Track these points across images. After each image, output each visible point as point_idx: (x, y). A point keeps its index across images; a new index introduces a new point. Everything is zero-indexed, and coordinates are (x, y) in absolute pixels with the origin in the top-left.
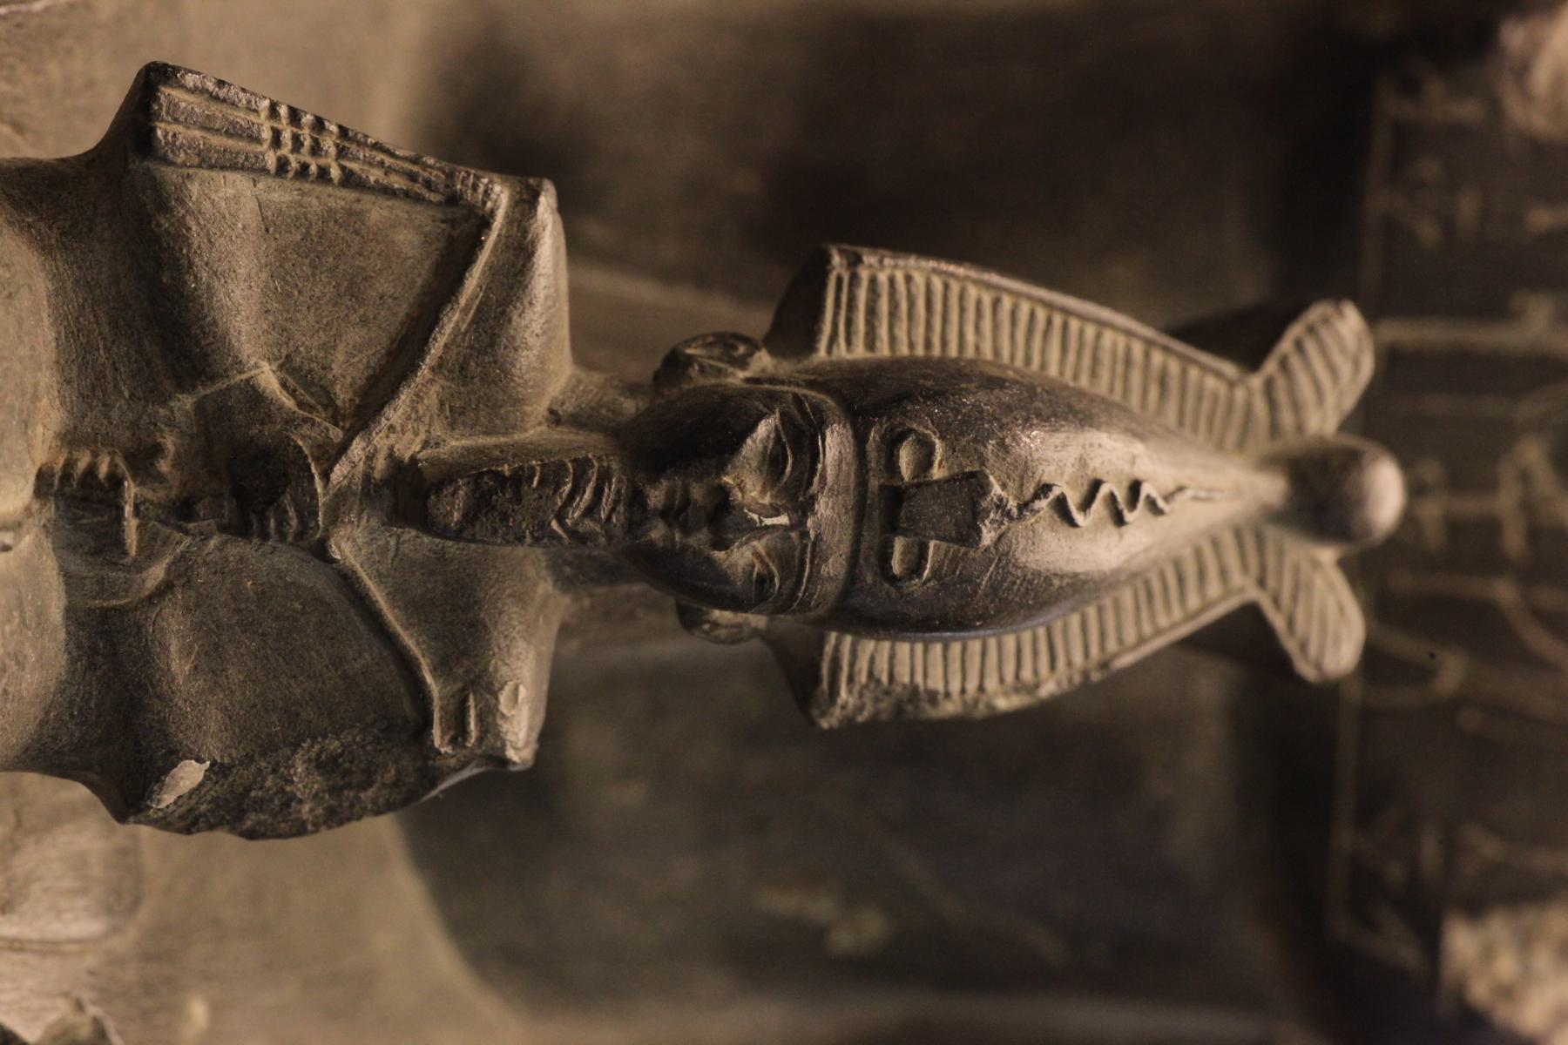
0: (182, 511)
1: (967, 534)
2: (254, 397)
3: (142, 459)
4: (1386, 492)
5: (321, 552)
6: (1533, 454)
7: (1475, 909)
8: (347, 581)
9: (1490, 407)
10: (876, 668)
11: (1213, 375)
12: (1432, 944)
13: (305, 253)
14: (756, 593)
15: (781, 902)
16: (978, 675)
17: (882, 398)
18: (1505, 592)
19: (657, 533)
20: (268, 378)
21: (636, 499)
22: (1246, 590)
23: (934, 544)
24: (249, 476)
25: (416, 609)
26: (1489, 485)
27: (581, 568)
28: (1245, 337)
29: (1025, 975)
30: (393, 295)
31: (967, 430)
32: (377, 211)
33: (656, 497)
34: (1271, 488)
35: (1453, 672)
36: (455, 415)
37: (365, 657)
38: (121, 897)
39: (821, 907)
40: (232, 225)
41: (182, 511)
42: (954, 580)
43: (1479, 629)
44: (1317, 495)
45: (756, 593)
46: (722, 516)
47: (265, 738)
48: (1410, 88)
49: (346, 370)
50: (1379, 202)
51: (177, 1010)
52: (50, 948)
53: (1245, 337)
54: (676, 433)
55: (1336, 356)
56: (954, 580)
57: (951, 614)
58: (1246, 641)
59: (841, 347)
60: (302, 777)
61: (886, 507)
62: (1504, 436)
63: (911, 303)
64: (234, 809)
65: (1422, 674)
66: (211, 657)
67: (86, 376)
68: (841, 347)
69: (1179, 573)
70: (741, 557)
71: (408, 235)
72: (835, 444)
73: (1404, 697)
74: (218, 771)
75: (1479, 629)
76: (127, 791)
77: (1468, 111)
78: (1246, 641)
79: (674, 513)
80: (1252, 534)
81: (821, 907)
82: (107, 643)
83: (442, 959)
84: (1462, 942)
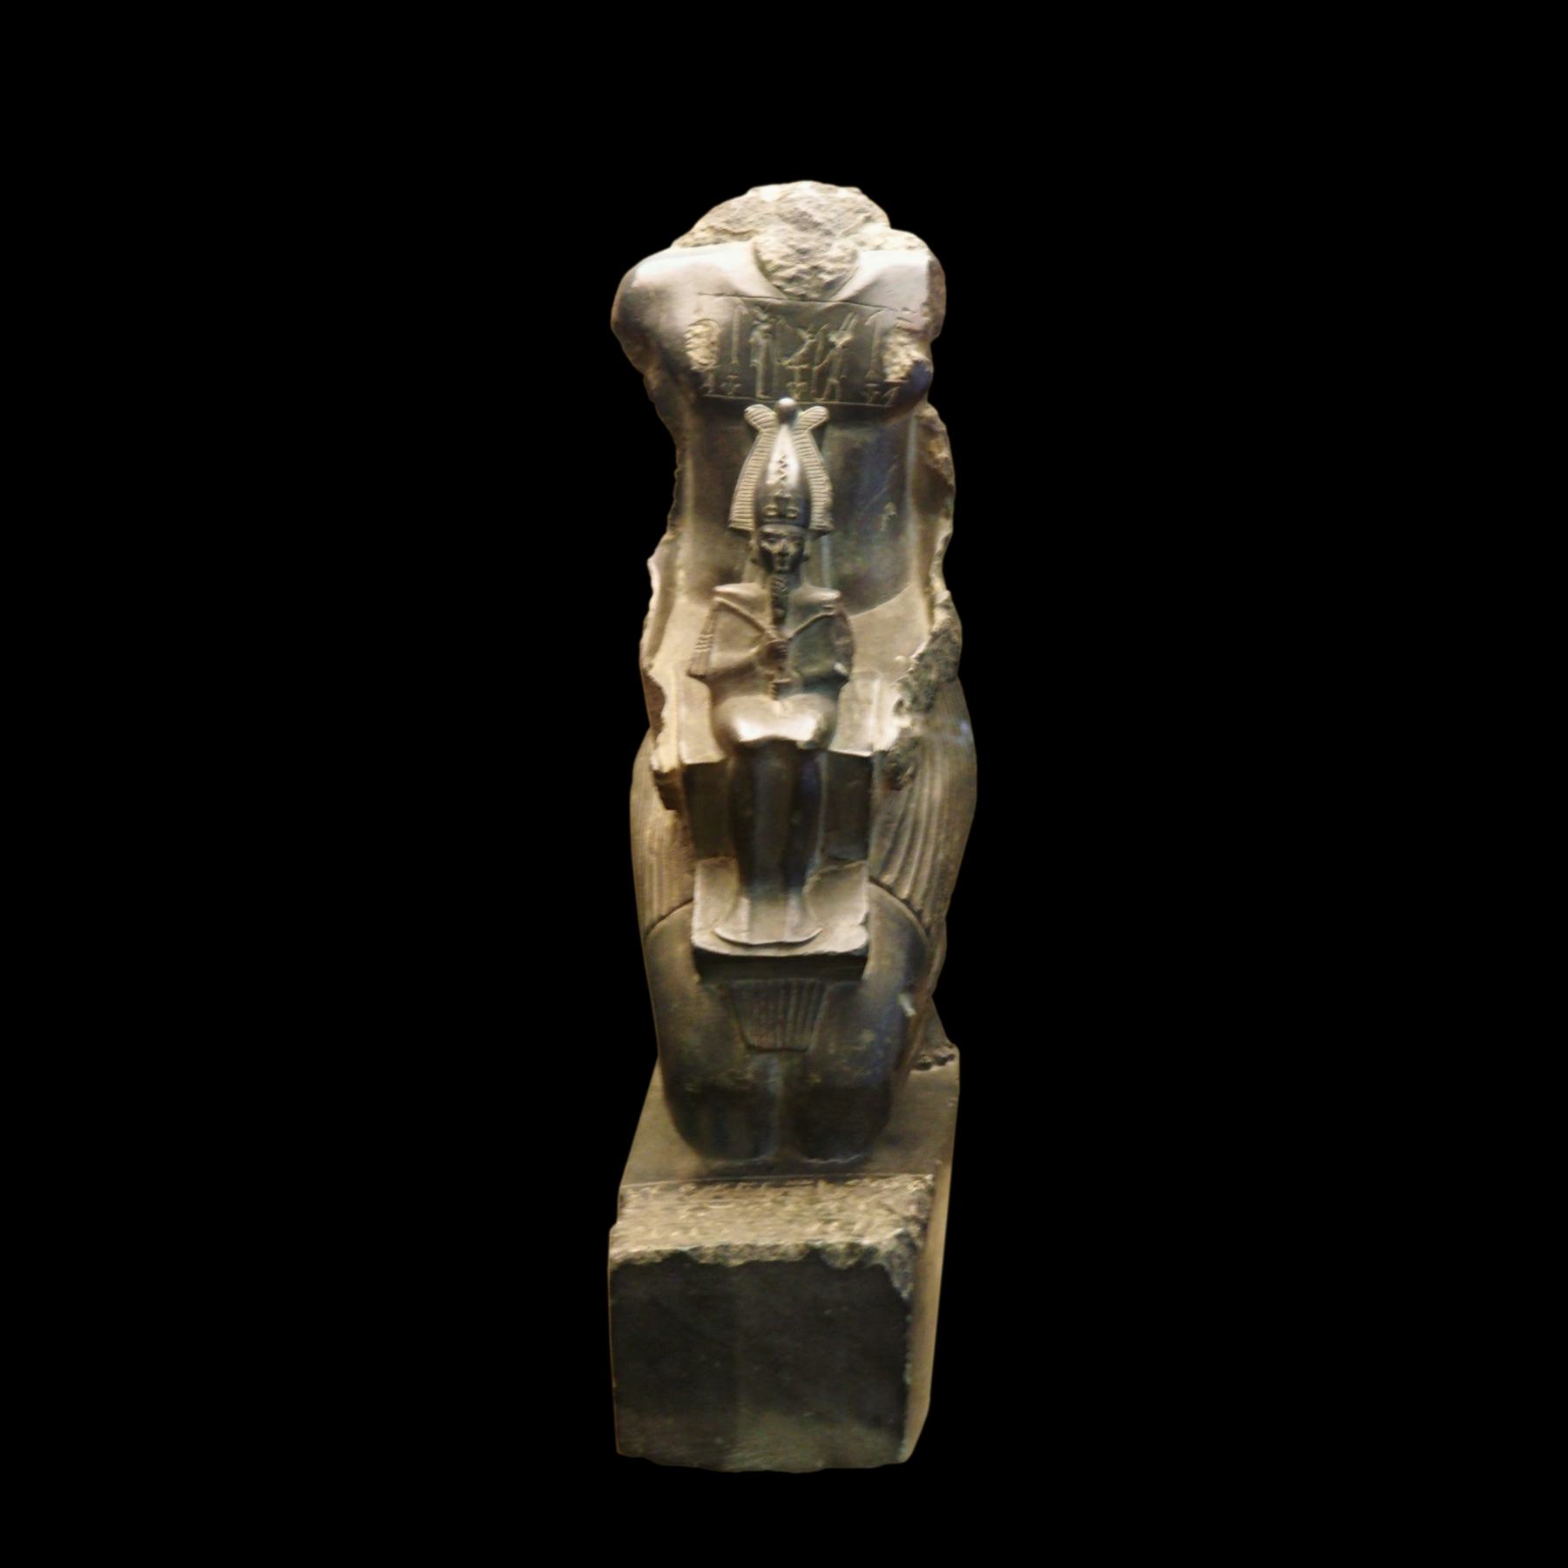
0: (781, 669)
1: (787, 500)
2: (758, 654)
3: (771, 678)
4: (786, 402)
5: (790, 639)
6: (786, 362)
7: (884, 376)
8: (799, 633)
9: (775, 372)
10: (819, 518)
11: (761, 440)
12: (892, 385)
13: (728, 640)
14: (801, 546)
15: (883, 526)
16: (822, 494)
17: (760, 519)
18: (816, 368)
19: (787, 567)
20: (754, 650)
21: (780, 572)
22: (806, 433)
23: (790, 508)
24: (774, 655)
25: (804, 617)
26: (792, 371)
27: (797, 582)
28: (753, 432)
29: (901, 473)
30: (737, 623)
31: (766, 500)
32: (720, 626)
33: (778, 568)
34: (784, 429)
35: (833, 380)
36: (762, 610)
37: (814, 629)
38: (870, 676)
39: (885, 518)
40: (720, 658)
41: (781, 669)
42: (797, 502)
43: (824, 374)
44: (787, 417)
45: (801, 546)
46: (783, 554)
47: (831, 651)
48: (707, 389)
49: (752, 633)
50: (730, 397)
51: (898, 663)
52: (881, 693)
53: (753, 432)
54: (766, 561)
55: (758, 413)
56: (797, 502)
57: (807, 503)
58: (819, 432)
59: (749, 525)
60: (840, 642)
61: (781, 517)
62: (782, 368)
63: (741, 511)
64: (848, 657)
65: (833, 387)
66: (812, 662)
67: (753, 689)
68: (749, 525)
69: (801, 450)
70: (792, 549)
71: (725, 619)
72: (768, 529)
73: (838, 390)
74: (839, 660)
75: (824, 374)
76: (841, 680)
77: (711, 376)
78: (819, 432)
79: (782, 564)
80: (794, 431)
81: (885, 518)
82: (809, 685)
83: (894, 601)
84: (892, 378)
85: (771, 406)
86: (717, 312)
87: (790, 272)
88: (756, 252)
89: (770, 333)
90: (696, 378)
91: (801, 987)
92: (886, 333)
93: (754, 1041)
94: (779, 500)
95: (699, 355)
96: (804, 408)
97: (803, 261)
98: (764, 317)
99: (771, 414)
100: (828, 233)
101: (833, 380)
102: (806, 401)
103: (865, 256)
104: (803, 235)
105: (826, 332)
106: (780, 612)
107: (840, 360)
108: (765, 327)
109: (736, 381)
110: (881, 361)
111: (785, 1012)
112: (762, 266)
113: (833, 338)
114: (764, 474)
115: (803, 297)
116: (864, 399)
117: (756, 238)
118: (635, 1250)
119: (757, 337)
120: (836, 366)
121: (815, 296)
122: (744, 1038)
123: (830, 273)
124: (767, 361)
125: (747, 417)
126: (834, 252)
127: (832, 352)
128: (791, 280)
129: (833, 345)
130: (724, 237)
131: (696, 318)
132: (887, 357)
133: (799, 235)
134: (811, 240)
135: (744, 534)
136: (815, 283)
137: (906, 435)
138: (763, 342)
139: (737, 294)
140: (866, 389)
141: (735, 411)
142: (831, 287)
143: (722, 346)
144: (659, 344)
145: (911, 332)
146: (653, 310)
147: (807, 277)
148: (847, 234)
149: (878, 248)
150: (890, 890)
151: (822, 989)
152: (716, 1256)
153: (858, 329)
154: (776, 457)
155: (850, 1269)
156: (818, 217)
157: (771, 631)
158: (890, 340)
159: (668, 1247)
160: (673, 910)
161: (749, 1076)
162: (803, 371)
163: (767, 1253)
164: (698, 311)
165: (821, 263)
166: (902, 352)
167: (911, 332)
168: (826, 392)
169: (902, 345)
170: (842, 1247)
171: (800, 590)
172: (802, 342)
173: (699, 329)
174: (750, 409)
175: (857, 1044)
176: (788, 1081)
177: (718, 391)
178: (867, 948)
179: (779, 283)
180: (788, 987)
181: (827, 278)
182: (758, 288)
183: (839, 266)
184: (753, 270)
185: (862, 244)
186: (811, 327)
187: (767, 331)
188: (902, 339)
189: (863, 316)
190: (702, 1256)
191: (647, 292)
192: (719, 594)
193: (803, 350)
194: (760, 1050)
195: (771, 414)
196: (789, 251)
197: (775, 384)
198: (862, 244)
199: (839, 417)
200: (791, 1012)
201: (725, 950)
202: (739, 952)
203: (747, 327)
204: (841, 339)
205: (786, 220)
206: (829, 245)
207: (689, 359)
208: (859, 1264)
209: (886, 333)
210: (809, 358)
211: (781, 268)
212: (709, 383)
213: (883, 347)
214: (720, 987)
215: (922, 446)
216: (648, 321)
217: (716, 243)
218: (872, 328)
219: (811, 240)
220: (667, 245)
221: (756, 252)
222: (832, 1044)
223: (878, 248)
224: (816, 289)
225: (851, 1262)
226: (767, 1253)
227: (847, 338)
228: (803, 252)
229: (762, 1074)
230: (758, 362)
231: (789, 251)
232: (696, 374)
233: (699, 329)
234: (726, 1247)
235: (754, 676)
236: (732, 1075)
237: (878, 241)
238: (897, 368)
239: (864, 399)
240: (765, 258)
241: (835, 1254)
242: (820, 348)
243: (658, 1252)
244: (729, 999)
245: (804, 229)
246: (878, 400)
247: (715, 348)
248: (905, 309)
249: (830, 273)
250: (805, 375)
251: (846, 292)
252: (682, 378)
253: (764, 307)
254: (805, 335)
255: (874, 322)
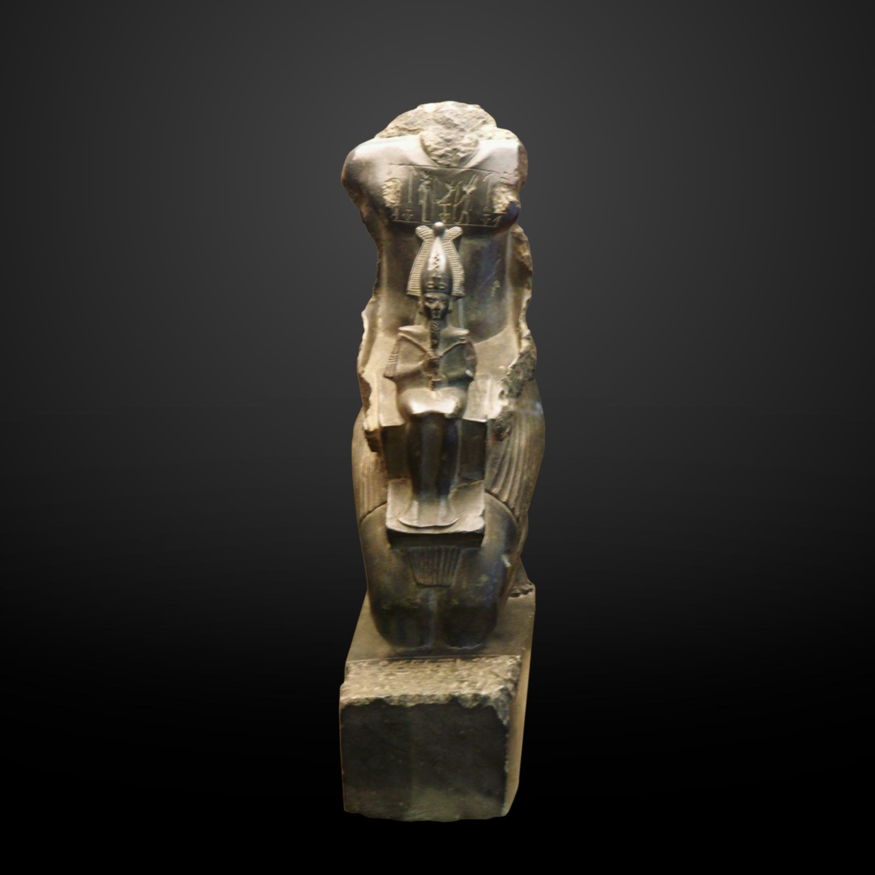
0: (436, 373)
1: (439, 279)
2: (423, 365)
3: (430, 378)
4: (439, 224)
5: (441, 357)
6: (439, 202)
7: (494, 210)
8: (446, 353)
9: (433, 208)
10: (457, 289)
11: (425, 246)
12: (498, 215)
13: (407, 357)
14: (447, 305)
15: (493, 294)
16: (458, 276)
17: (424, 289)
18: (455, 205)
19: (439, 317)
20: (421, 363)
21: (435, 319)
22: (450, 242)
23: (441, 284)
24: (432, 365)
25: (449, 344)
26: (442, 207)
27: (445, 325)
28: (420, 241)
29: (503, 264)
30: (412, 347)
31: (427, 279)
32: (402, 349)
33: (434, 317)
34: (438, 239)
35: (465, 212)
36: (425, 340)
37: (454, 351)
38: (486, 377)
39: (494, 289)
40: (402, 367)
41: (436, 373)
42: (445, 280)
43: (460, 209)
44: (439, 233)
45: (447, 305)
46: (437, 309)
47: (464, 363)
48: (394, 217)
49: (420, 353)
50: (408, 221)
51: (501, 370)
52: (492, 387)
53: (420, 241)
54: (428, 313)
55: (423, 230)
56: (445, 280)
57: (450, 281)
58: (457, 241)
59: (418, 293)
60: (469, 358)
61: (436, 289)
62: (436, 205)
63: (414, 285)
64: (473, 366)
65: (465, 216)
66: (453, 370)
67: (420, 385)
68: (418, 293)
69: (447, 251)
70: (442, 306)
71: (405, 346)
72: (429, 295)
73: (468, 218)
74: (468, 369)
75: (460, 209)
76: (469, 379)
77: (397, 210)
78: (457, 241)
79: (437, 315)
80: (443, 240)
81: (494, 289)
82: (452, 382)
83: (499, 335)
84: (498, 211)
89: (430, 186)
90: (389, 211)
91: (447, 551)
93: (421, 581)
94: (434, 279)
95: (390, 198)
96: (449, 228)
97: (448, 146)
98: (426, 177)
101: (465, 212)
102: (450, 224)
105: (461, 185)
106: (435, 341)
107: (469, 201)
108: (427, 182)
110: (491, 202)
111: (438, 565)
113: (465, 189)
114: (426, 264)
115: (448, 166)
116: (482, 223)
118: (354, 697)
119: (423, 188)
121: (455, 165)
122: (415, 579)
123: (463, 152)
124: (428, 201)
127: (464, 197)
128: (441, 156)
129: (465, 193)
130: (404, 132)
131: (389, 177)
132: (495, 199)
134: (452, 134)
135: (415, 298)
136: (455, 158)
138: (426, 191)
139: (411, 164)
142: (464, 160)
143: (403, 193)
150: (497, 497)
151: (459, 552)
152: (399, 701)
153: (479, 184)
154: (433, 255)
155: (475, 708)
156: (456, 121)
157: (430, 352)
159: (372, 696)
160: (376, 508)
161: (418, 601)
162: (448, 207)
163: (428, 699)
165: (458, 147)
168: (461, 219)
170: (470, 696)
171: (446, 329)
172: (448, 191)
173: (390, 184)
175: (478, 583)
176: (439, 604)
177: (401, 218)
179: (435, 158)
180: (439, 551)
186: (453, 182)
190: (392, 701)
192: (401, 331)
193: (448, 196)
194: (424, 586)
197: (433, 214)
200: (442, 565)
201: (405, 530)
202: (412, 531)
204: (469, 189)
205: (439, 123)
206: (463, 137)
208: (480, 706)
209: (494, 186)
211: (436, 149)
212: (396, 214)
214: (402, 551)
217: (400, 135)
220: (372, 137)
222: (464, 583)
224: (455, 161)
225: (475, 704)
226: (428, 699)
227: (473, 188)
228: (448, 141)
229: (425, 599)
230: (423, 202)
231: (440, 140)
232: (388, 209)
233: (390, 184)
234: (405, 696)
235: (421, 377)
236: (408, 600)
241: (466, 700)
242: (458, 194)
243: (367, 699)
244: (407, 558)
245: (449, 128)
247: (399, 194)
249: (463, 152)
250: (449, 209)
251: (472, 163)
252: (381, 211)
253: (426, 171)
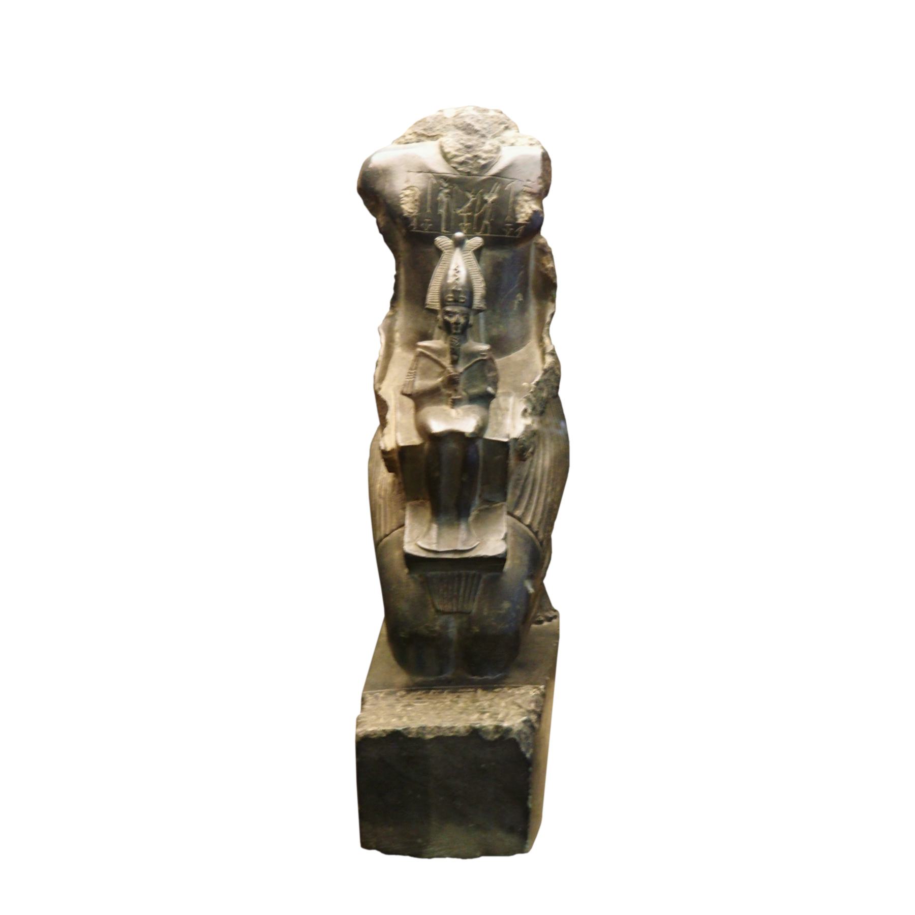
0: (456, 391)
1: (459, 292)
2: (442, 381)
3: (450, 395)
4: (459, 235)
5: (461, 373)
6: (459, 211)
7: (516, 219)
8: (466, 369)
9: (452, 217)
10: (478, 302)
11: (444, 257)
12: (521, 224)
13: (425, 374)
14: (467, 319)
15: (516, 307)
16: (479, 288)
17: (444, 303)
18: (476, 215)
19: (459, 331)
20: (440, 379)
21: (455, 334)
22: (470, 253)
23: (461, 297)
24: (452, 382)
25: (469, 360)
26: (462, 217)
27: (465, 339)
28: (439, 252)
29: (526, 276)
30: (430, 363)
31: (447, 292)
32: (420, 365)
33: (454, 331)
34: (458, 250)
35: (486, 222)
36: (444, 356)
37: (475, 367)
38: (508, 394)
39: (516, 302)
40: (420, 384)
41: (456, 391)
42: (465, 293)
43: (481, 218)
44: (459, 243)
45: (467, 319)
46: (457, 323)
47: (485, 380)
48: (412, 227)
49: (439, 370)
50: (426, 231)
51: (524, 387)
52: (514, 404)
53: (439, 252)
54: (447, 328)
55: (442, 241)
56: (465, 293)
57: (471, 294)
58: (478, 252)
59: (437, 306)
60: (490, 375)
61: (456, 302)
62: (456, 215)
63: (433, 298)
64: (495, 383)
65: (486, 226)
66: (474, 386)
67: (439, 402)
68: (437, 306)
69: (468, 262)
70: (462, 320)
71: (423, 361)
72: (448, 309)
73: (489, 228)
74: (489, 385)
75: (481, 218)
76: (491, 397)
77: (415, 220)
78: (478, 252)
79: (457, 329)
80: (464, 251)
81: (516, 302)
82: (472, 399)
83: (522, 350)
84: (520, 221)
85: (450, 237)
86: (418, 182)
87: (461, 159)
88: (441, 147)
89: (449, 194)
90: (406, 220)
91: (467, 576)
92: (517, 194)
93: (440, 607)
94: (454, 292)
96: (469, 238)
97: (468, 152)
98: (446, 185)
99: (450, 242)
100: (483, 136)
101: (486, 222)
102: (470, 234)
103: (505, 149)
104: (469, 137)
105: (482, 194)
106: (455, 357)
107: (490, 210)
108: (447, 191)
109: (429, 223)
110: (514, 211)
111: (458, 591)
112: (445, 155)
113: (486, 197)
114: (446, 277)
115: (469, 174)
116: (504, 233)
117: (441, 139)
118: (370, 729)
119: (442, 196)
120: (488, 214)
121: (475, 172)
122: (434, 606)
123: (484, 159)
124: (448, 211)
125: (436, 243)
126: (487, 147)
127: (485, 206)
128: (462, 163)
129: (486, 201)
130: (422, 138)
131: (406, 185)
132: (518, 208)
133: (466, 137)
134: (473, 140)
135: (434, 312)
136: (475, 165)
137: (529, 254)
138: (445, 200)
139: (430, 172)
140: (505, 227)
141: (429, 240)
142: (485, 167)
143: (422, 202)
144: (385, 201)
145: (532, 194)
146: (381, 181)
147: (471, 162)
148: (494, 136)
149: (512, 145)
150: (520, 519)
151: (480, 577)
152: (418, 733)
153: (500, 192)
154: (453, 267)
155: (496, 740)
156: (477, 127)
157: (450, 368)
158: (520, 198)
159: (390, 728)
160: (393, 531)
161: (437, 628)
162: (468, 216)
163: (447, 731)
164: (407, 181)
165: (479, 153)
166: (526, 205)
167: (532, 194)
168: (482, 229)
169: (526, 201)
170: (491, 728)
171: (467, 344)
172: (468, 200)
173: (408, 192)
174: (438, 239)
175: (500, 609)
176: (460, 631)
177: (419, 228)
178: (506, 553)
179: (455, 165)
180: (460, 576)
181: (483, 162)
182: (442, 168)
183: (490, 155)
184: (439, 157)
185: (503, 142)
186: (473, 191)
187: (447, 193)
188: (526, 198)
189: (503, 184)
190: (410, 733)
191: (378, 171)
192: (420, 347)
193: (468, 204)
194: (444, 613)
195: (450, 242)
196: (461, 146)
197: (452, 224)
198: (503, 142)
199: (489, 243)
200: (462, 590)
201: (423, 554)
202: (431, 556)
203: (436, 191)
204: (491, 198)
205: (459, 128)
206: (484, 143)
207: (402, 209)
208: (501, 738)
209: (517, 194)
210: (472, 209)
211: (456, 156)
212: (414, 223)
213: (515, 202)
214: (420, 576)
215: (538, 260)
216: (378, 187)
217: (418, 142)
218: (509, 191)
219: (473, 140)
221: (441, 147)
222: (486, 609)
223: (512, 145)
224: (476, 169)
225: (496, 736)
226: (447, 731)
227: (494, 197)
228: (469, 147)
229: (445, 627)
230: (442, 211)
231: (461, 146)
232: (406, 218)
233: (408, 192)
234: (424, 728)
235: (440, 395)
236: (427, 627)
237: (512, 141)
238: (523, 215)
239: (504, 233)
240: (446, 150)
241: (487, 732)
242: (478, 203)
243: (384, 731)
244: (426, 583)
245: (469, 134)
246: (513, 233)
247: (417, 203)
248: (528, 180)
249: (484, 159)
250: (470, 219)
251: (494, 170)
252: (398, 220)
253: (446, 179)
254: (470, 196)
255: (510, 188)
